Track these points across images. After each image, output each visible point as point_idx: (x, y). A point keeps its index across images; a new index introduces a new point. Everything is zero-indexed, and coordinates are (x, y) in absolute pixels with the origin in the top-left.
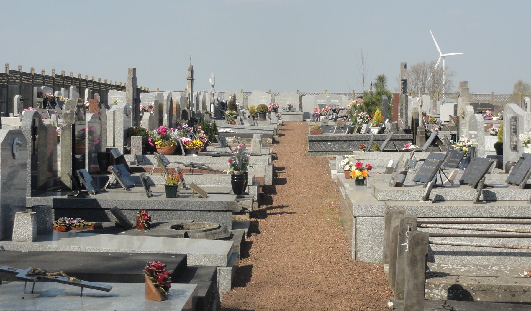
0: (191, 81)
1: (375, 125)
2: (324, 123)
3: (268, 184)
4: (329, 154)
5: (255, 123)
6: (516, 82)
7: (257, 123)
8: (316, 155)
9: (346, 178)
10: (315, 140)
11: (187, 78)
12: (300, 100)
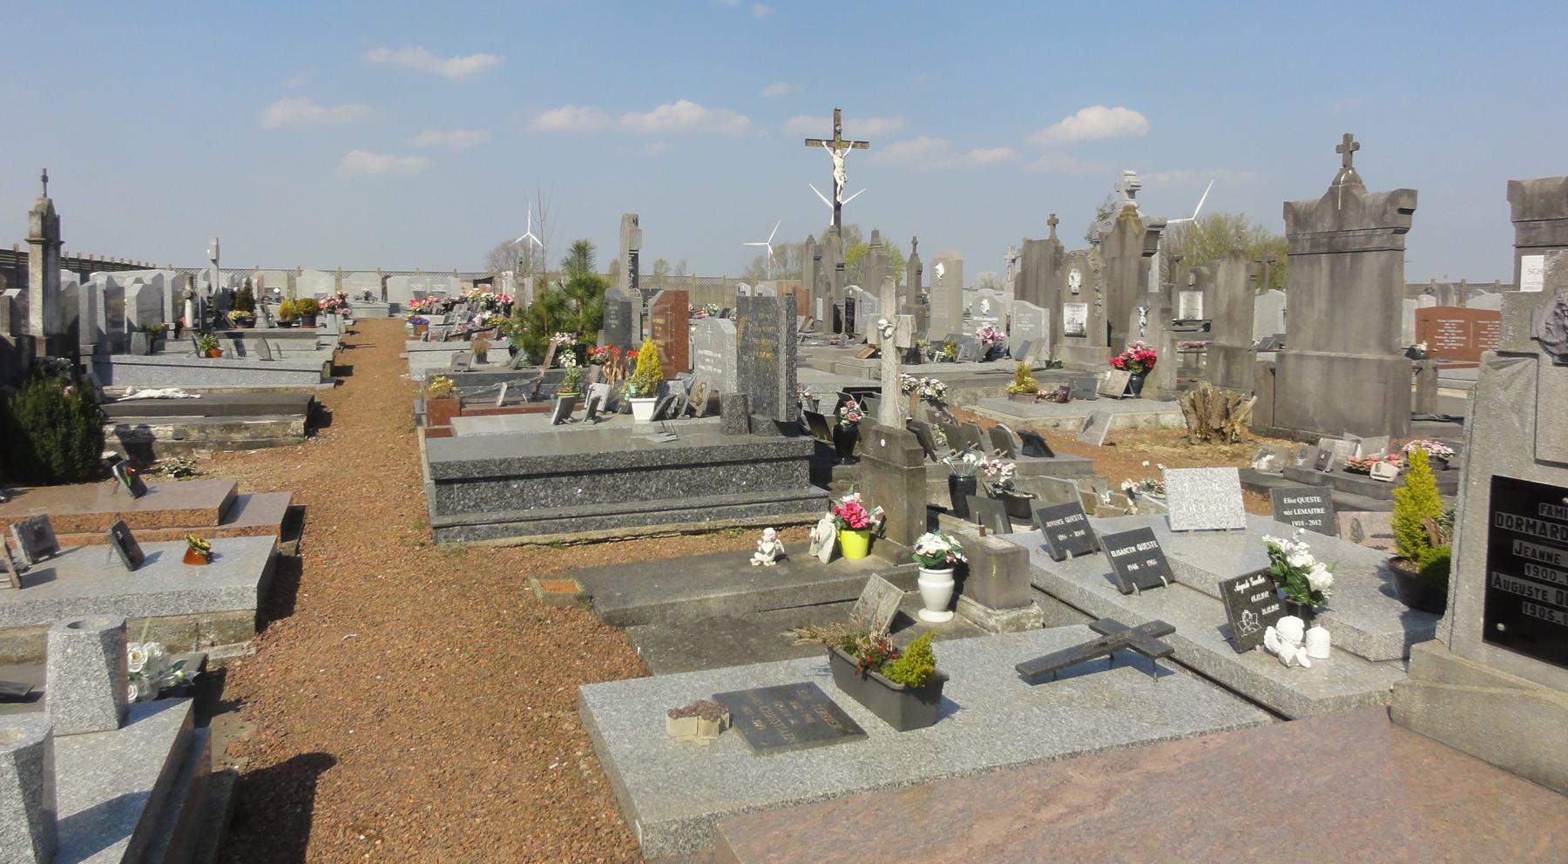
1: (645, 390)
2: (459, 364)
4: (518, 532)
6: (611, 261)
8: (467, 539)
10: (460, 475)
11: (28, 237)
12: (384, 283)
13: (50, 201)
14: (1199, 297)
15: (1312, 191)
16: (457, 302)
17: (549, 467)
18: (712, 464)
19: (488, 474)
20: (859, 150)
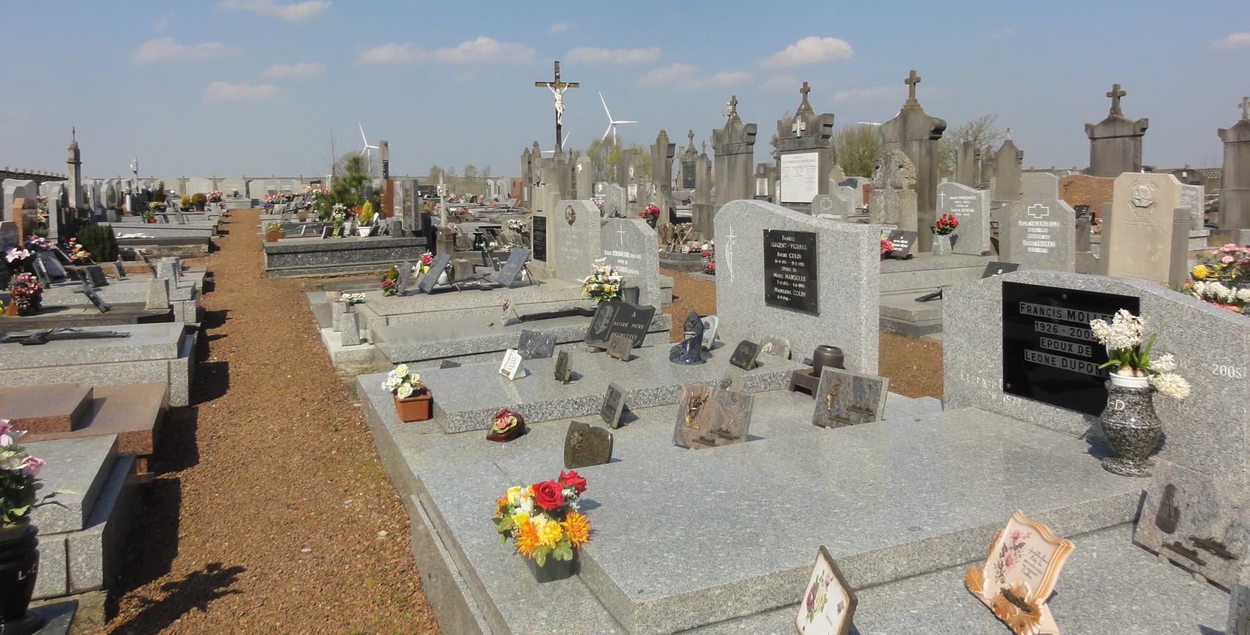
0: (74, 165)
1: (365, 223)
3: (180, 405)
4: (300, 273)
5: (185, 219)
6: (431, 167)
7: (188, 220)
8: (280, 275)
9: (405, 422)
12: (247, 185)
13: (77, 142)
14: (766, 181)
15: (721, 125)
16: (297, 196)
17: (313, 248)
18: (382, 248)
19: (288, 251)
20: (573, 89)
